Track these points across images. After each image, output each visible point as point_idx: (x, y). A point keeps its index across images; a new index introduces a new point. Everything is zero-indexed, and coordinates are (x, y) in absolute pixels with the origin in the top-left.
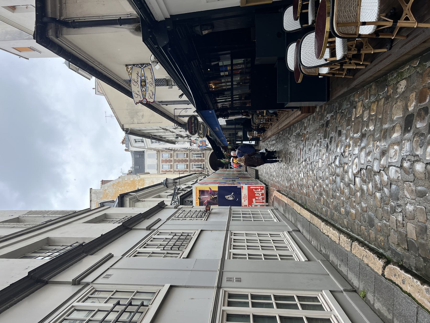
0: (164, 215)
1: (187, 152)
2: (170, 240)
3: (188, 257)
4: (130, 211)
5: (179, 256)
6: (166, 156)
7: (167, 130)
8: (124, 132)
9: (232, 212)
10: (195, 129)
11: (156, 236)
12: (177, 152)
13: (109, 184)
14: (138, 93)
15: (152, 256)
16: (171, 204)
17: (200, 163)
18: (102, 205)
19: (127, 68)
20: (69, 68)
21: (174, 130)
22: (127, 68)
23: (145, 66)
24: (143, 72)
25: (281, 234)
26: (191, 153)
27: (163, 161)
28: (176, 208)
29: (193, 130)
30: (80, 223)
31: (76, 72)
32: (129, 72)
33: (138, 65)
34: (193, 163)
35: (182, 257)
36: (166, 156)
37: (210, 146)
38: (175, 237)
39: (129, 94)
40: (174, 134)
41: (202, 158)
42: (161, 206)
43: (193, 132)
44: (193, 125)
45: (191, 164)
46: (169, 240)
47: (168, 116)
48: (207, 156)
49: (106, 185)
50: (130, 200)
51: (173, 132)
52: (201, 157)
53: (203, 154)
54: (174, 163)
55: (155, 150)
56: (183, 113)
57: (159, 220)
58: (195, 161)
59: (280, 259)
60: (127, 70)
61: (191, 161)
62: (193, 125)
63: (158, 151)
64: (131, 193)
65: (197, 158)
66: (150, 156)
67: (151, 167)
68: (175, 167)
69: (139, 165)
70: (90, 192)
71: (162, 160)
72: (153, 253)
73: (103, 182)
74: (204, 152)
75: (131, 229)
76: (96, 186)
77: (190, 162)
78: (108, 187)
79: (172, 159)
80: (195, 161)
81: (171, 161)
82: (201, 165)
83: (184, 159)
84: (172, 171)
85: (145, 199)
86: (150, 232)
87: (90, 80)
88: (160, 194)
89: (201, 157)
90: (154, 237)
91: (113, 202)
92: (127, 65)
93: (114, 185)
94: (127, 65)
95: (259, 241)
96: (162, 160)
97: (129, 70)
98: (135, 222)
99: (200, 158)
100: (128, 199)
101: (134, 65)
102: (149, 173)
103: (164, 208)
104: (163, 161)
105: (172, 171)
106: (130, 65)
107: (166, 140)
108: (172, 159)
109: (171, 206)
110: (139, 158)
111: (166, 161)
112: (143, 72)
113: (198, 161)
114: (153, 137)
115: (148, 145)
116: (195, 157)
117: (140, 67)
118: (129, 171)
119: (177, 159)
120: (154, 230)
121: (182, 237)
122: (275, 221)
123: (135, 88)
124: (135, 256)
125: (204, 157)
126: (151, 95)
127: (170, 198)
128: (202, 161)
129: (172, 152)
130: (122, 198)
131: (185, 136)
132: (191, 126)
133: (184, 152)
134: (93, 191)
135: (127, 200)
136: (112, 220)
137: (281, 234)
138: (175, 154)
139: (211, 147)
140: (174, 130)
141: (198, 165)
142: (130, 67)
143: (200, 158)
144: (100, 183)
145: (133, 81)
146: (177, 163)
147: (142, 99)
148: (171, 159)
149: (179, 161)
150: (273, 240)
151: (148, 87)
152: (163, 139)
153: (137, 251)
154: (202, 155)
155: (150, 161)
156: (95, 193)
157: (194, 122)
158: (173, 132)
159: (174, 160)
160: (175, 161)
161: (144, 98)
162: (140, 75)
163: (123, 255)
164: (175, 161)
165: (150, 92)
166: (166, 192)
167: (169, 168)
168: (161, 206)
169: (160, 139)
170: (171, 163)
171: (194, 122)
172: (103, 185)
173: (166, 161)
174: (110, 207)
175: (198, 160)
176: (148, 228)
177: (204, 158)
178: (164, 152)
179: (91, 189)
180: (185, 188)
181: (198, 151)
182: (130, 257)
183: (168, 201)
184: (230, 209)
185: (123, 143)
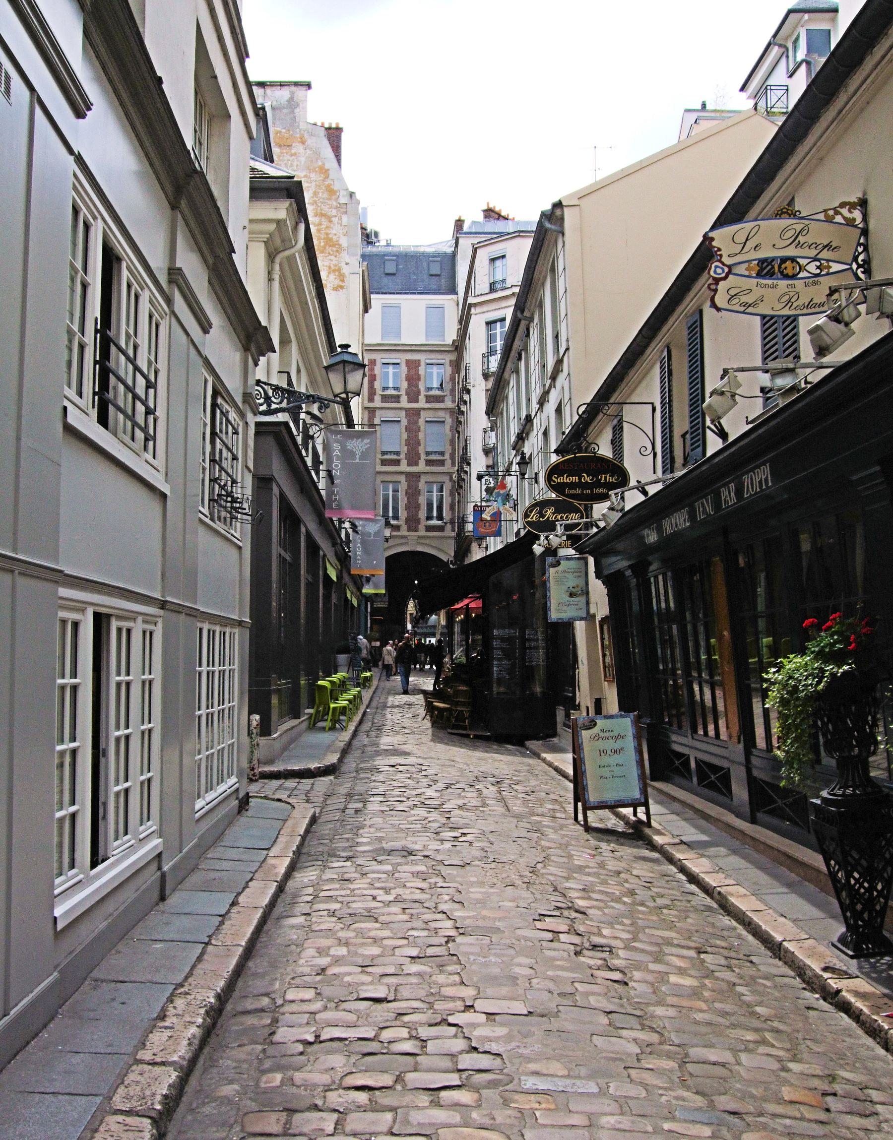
0: (221, 346)
1: (449, 462)
2: (132, 361)
3: (69, 429)
4: (240, 214)
5: (72, 393)
6: (434, 376)
7: (554, 378)
8: (549, 207)
9: (228, 630)
10: (572, 485)
11: (145, 307)
12: (449, 420)
13: (328, 152)
14: (750, 244)
15: (73, 279)
16: (258, 382)
17: (403, 514)
18: (260, 113)
19: (852, 206)
20: (790, 12)
21: (550, 407)
22: (852, 206)
23: (862, 276)
24: (835, 267)
25: (152, 826)
26: (446, 479)
27: (413, 365)
28: (247, 397)
29: (565, 479)
30: (196, 9)
31: (775, 36)
32: (837, 213)
33: (866, 249)
34: (403, 486)
35: (66, 403)
36: (434, 376)
37: (477, 554)
38: (141, 382)
39: (733, 213)
40: (535, 406)
41: (424, 523)
42: (253, 339)
43: (561, 480)
44: (586, 478)
45: (403, 479)
46: (131, 354)
47: (622, 379)
49: (326, 142)
50: (278, 222)
51: (542, 402)
52: (429, 518)
54: (407, 410)
55: (463, 332)
56: (632, 441)
57: (206, 327)
58: (413, 493)
59: (59, 814)
60: (843, 205)
61: (413, 478)
62: (586, 478)
63: (459, 347)
64: (302, 227)
65: (422, 500)
66: (435, 314)
67: (392, 316)
68: (390, 415)
69: (392, 272)
70: (296, 84)
71: (417, 363)
72: (85, 286)
73: (334, 135)
74: (449, 532)
75: (174, 206)
76: (318, 110)
77: (408, 475)
78: (317, 154)
79: (422, 403)
80: (413, 493)
81: (413, 396)
83: (421, 450)
84: (371, 400)
85: (276, 285)
86: (163, 279)
87: (742, 89)
88: (294, 346)
89: (429, 518)
90: (145, 296)
91: (269, 158)
92: (863, 203)
93: (324, 172)
94: (863, 203)
95: (146, 727)
96: (417, 363)
97: (845, 211)
98: (201, 225)
99: (422, 514)
100: (282, 214)
101: (865, 232)
102: (366, 310)
103: (246, 349)
104: (413, 365)
105: (371, 400)
106: (865, 218)
107: (506, 375)
108: (422, 403)
109: (251, 382)
110: (432, 273)
111: (413, 378)
112: (835, 267)
113: (412, 506)
114: (523, 324)
115: (479, 309)
116: (428, 494)
117: (855, 259)
118: (376, 234)
119: (421, 422)
120: (169, 301)
121: (140, 408)
122: (199, 804)
123: (766, 236)
124: (76, 211)
125: (429, 528)
126: (744, 299)
127: (277, 380)
128: (413, 523)
130: (291, 190)
131: (527, 450)
132: (584, 470)
133: (448, 450)
134: (300, 92)
135: (280, 210)
136: (204, 142)
137: (152, 826)
138: (441, 414)
139: (467, 562)
140: (550, 407)
141: (396, 509)
142: (857, 215)
143: (422, 514)
144: (331, 121)
145: (799, 228)
146: (404, 422)
147: (727, 260)
148: (422, 398)
149: (412, 429)
150: (127, 791)
151: (774, 287)
152: (510, 365)
153: (95, 218)
154: (435, 522)
155: (416, 319)
156: (291, 99)
157: (598, 484)
158: (542, 402)
159: (418, 411)
160: (413, 414)
161: (730, 267)
162: (825, 254)
163: (80, 160)
164: (413, 414)
165: (757, 293)
166: (299, 371)
167: (385, 388)
168: (253, 339)
169: (513, 354)
170: (404, 398)
171: (598, 484)
172: (322, 132)
173: (413, 378)
174: (251, 138)
175: (418, 507)
176: (175, 275)
177: (422, 532)
178: (449, 370)
179: (308, 86)
180: (314, 448)
181: (452, 508)
182: (75, 188)
183: (269, 369)
184: (240, 623)
185: (490, 213)
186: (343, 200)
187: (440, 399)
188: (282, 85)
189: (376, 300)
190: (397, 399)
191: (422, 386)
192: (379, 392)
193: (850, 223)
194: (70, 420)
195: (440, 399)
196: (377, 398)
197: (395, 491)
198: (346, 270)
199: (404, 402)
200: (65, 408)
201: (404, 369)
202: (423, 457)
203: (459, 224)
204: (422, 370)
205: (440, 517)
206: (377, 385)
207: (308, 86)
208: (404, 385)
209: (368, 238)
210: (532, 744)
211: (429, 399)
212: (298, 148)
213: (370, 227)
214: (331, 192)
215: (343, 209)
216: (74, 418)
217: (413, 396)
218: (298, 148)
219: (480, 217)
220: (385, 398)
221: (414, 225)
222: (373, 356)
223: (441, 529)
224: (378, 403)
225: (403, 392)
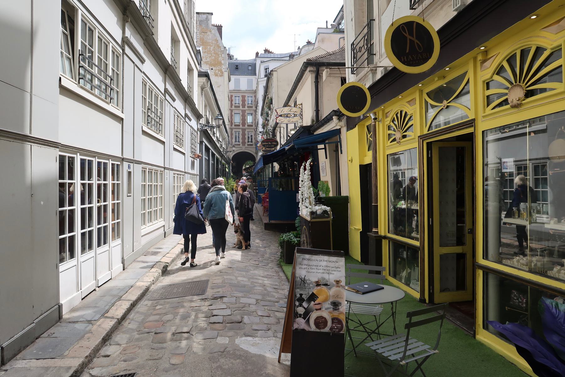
6: (249, 100)
17: (241, 141)
27: (243, 97)
34: (241, 133)
45: (241, 130)
48: (249, 149)
49: (217, 31)
52: (248, 142)
53: (252, 145)
65: (246, 137)
66: (250, 82)
67: (237, 82)
68: (237, 112)
70: (208, 13)
74: (254, 146)
80: (244, 135)
81: (244, 106)
82: (251, 142)
89: (248, 142)
93: (217, 41)
99: (246, 141)
102: (229, 81)
104: (243, 97)
110: (248, 69)
111: (244, 101)
113: (244, 138)
119: (246, 114)
125: (248, 145)
128: (244, 143)
129: (254, 108)
134: (209, 16)
141: (252, 139)
143: (246, 141)
144: (218, 23)
146: (241, 114)
148: (246, 107)
154: (250, 143)
156: (207, 18)
159: (245, 110)
160: (244, 112)
164: (244, 112)
170: (241, 107)
173: (244, 101)
177: (246, 145)
179: (212, 14)
185: (266, 51)
186: (222, 50)
187: (251, 107)
188: (204, 13)
189: (233, 78)
190: (239, 107)
191: (246, 103)
192: (234, 105)
193: (300, 108)
194: (63, 83)
195: (251, 107)
196: (233, 107)
197: (239, 134)
198: (223, 70)
199: (241, 126)
200: (60, 78)
201: (241, 98)
202: (247, 105)
203: (257, 54)
204: (246, 98)
205: (251, 142)
206: (233, 103)
207: (212, 14)
208: (241, 103)
209: (230, 57)
210: (187, 106)
211: (248, 107)
212: (209, 33)
213: (231, 53)
214: (219, 47)
215: (223, 52)
216: (65, 83)
217: (244, 106)
218: (209, 33)
219: (263, 52)
220: (235, 107)
221: (244, 53)
222: (232, 94)
223: (252, 145)
224: (233, 126)
225: (241, 105)
